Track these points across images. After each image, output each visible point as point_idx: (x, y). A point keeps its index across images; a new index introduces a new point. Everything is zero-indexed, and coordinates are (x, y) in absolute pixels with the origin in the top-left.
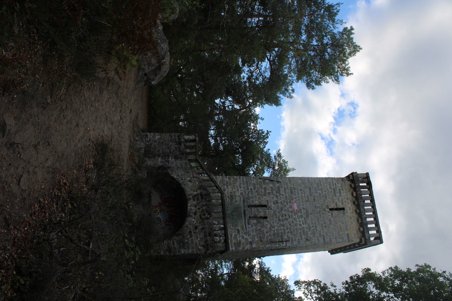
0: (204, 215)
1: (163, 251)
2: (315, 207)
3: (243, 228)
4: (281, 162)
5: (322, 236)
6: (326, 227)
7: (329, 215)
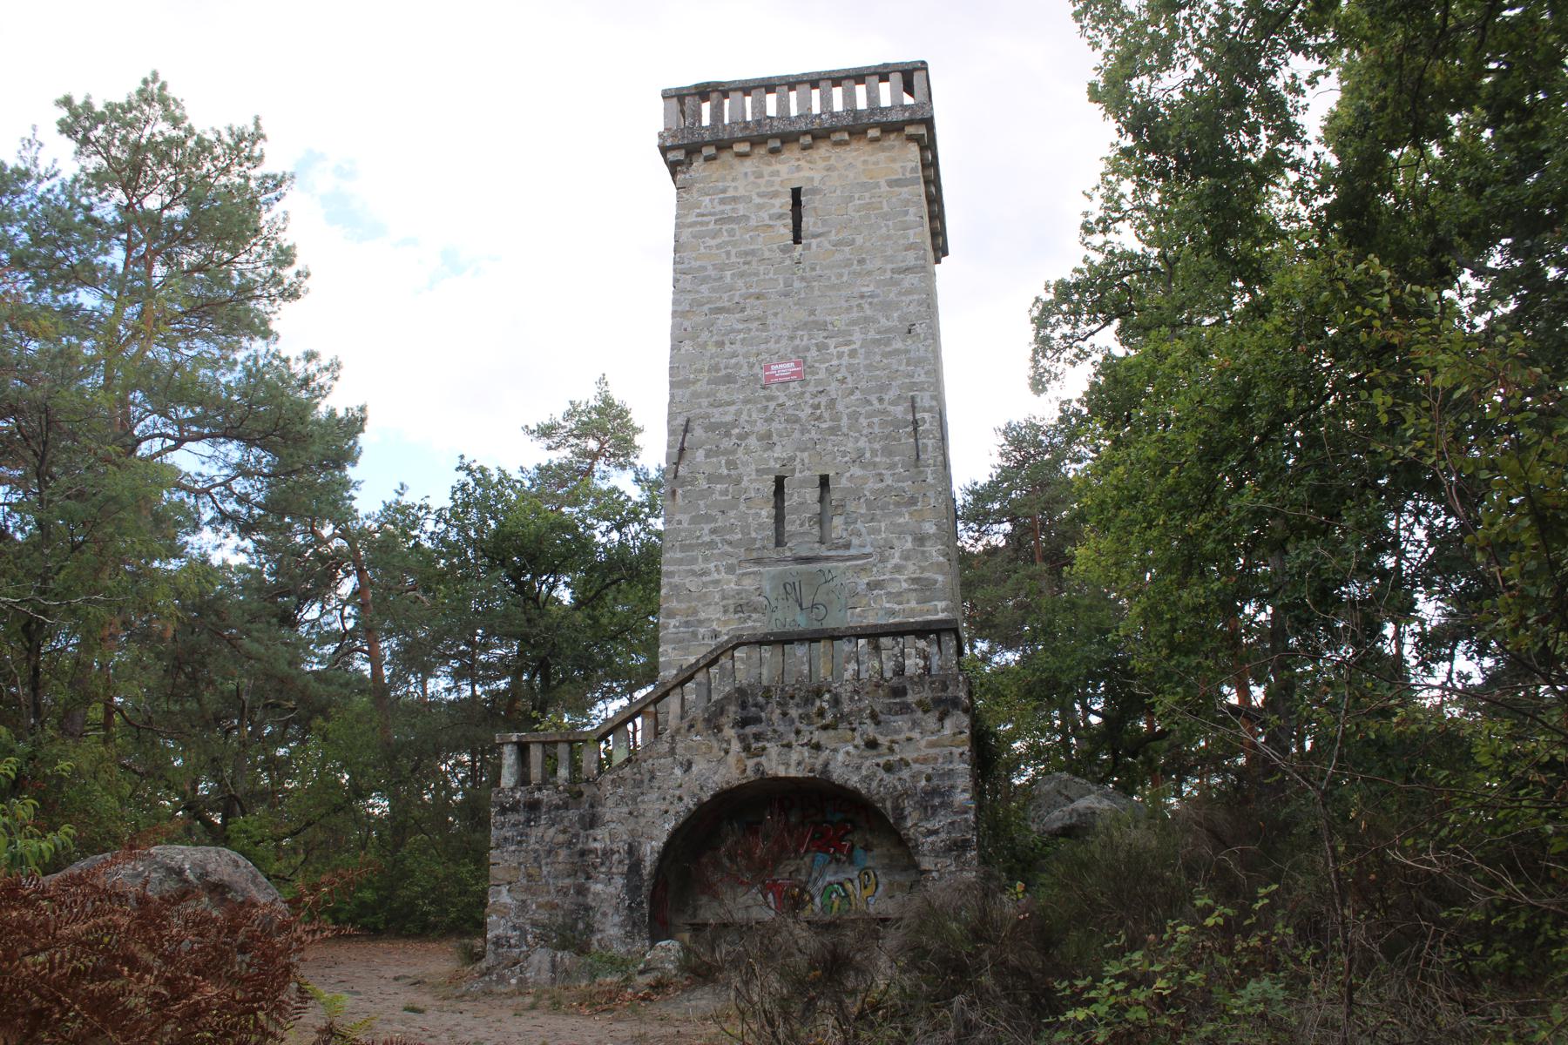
0: (821, 713)
1: (961, 870)
2: (786, 295)
4: (571, 425)
6: (861, 261)
7: (818, 246)
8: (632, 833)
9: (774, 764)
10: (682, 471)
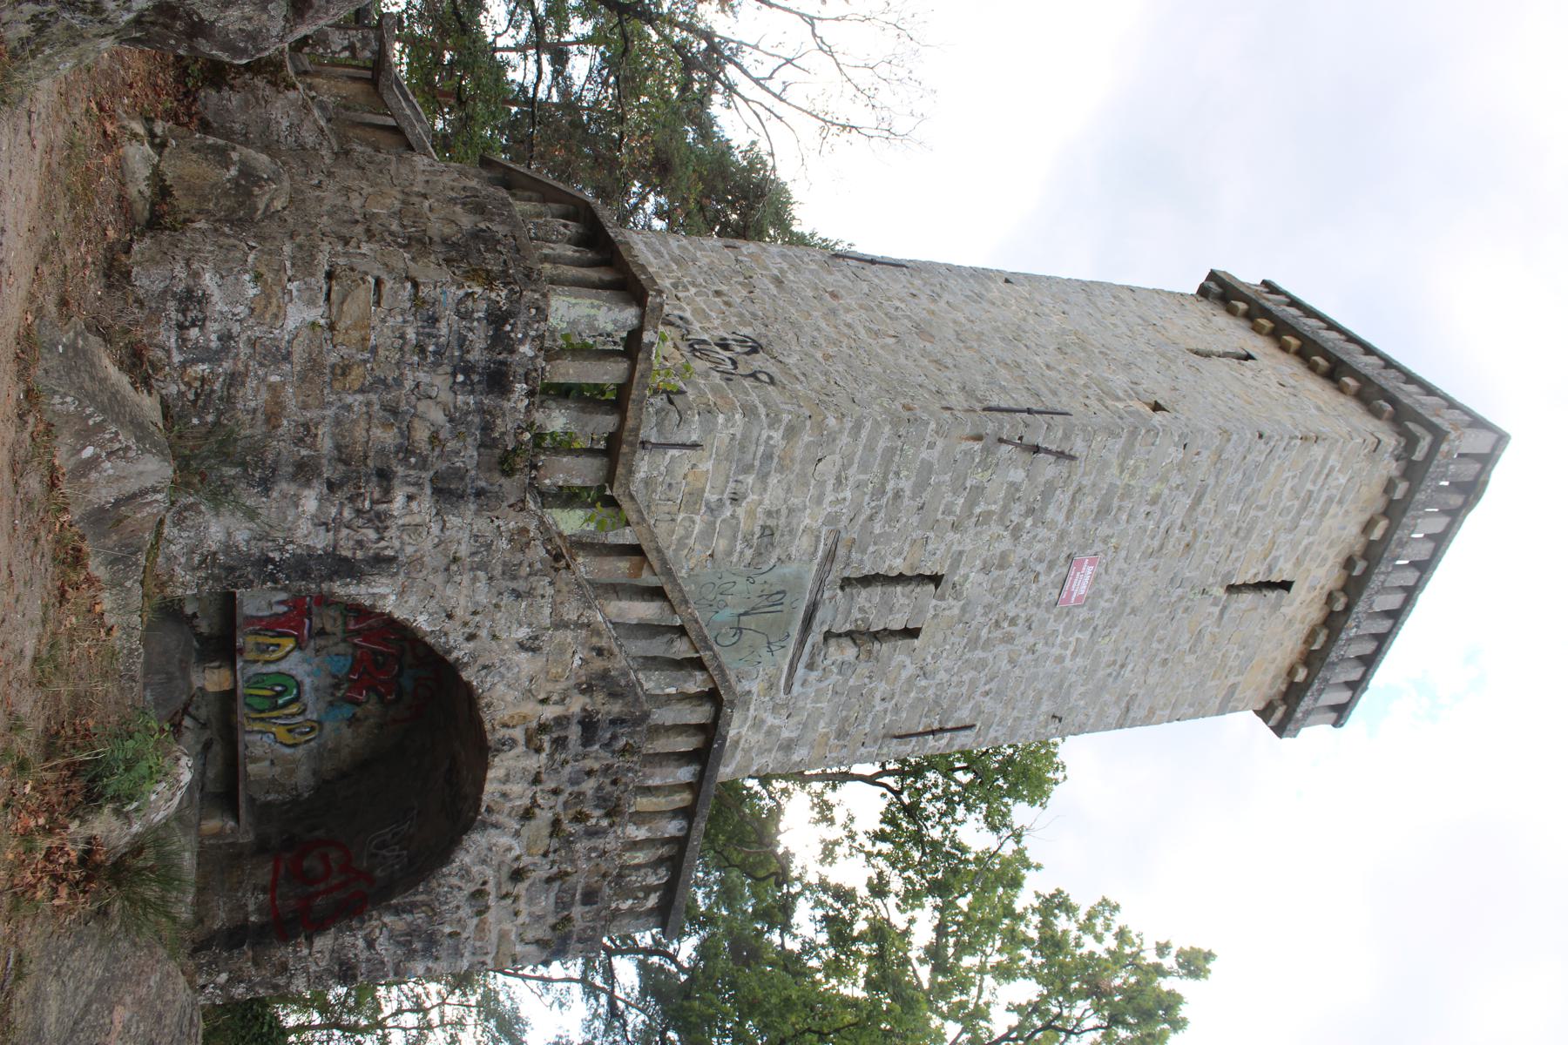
0: (580, 818)
8: (417, 562)
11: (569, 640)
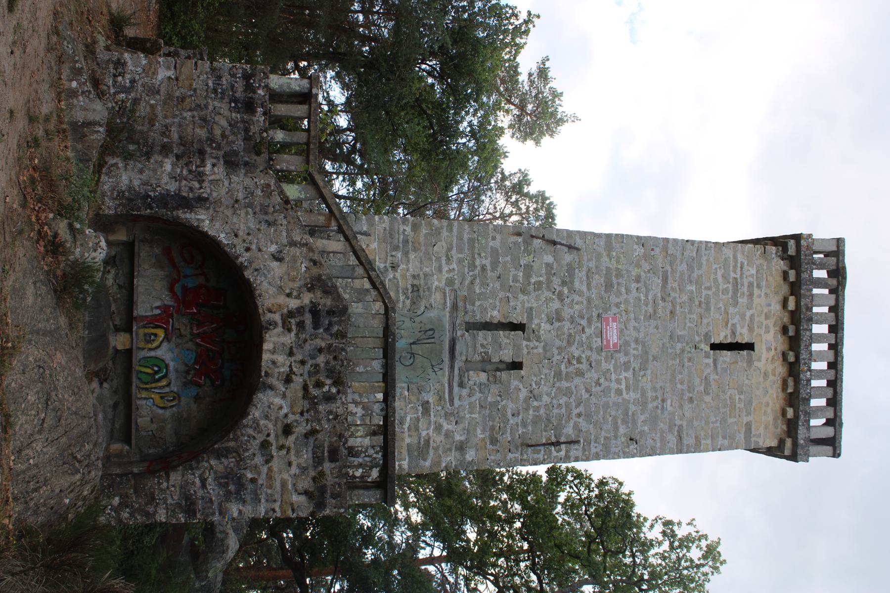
0: (319, 385)
1: (167, 509)
2: (671, 337)
3: (441, 398)
5: (677, 428)
6: (691, 400)
7: (707, 364)
8: (218, 202)
9: (275, 339)
10: (537, 243)
11: (298, 254)
